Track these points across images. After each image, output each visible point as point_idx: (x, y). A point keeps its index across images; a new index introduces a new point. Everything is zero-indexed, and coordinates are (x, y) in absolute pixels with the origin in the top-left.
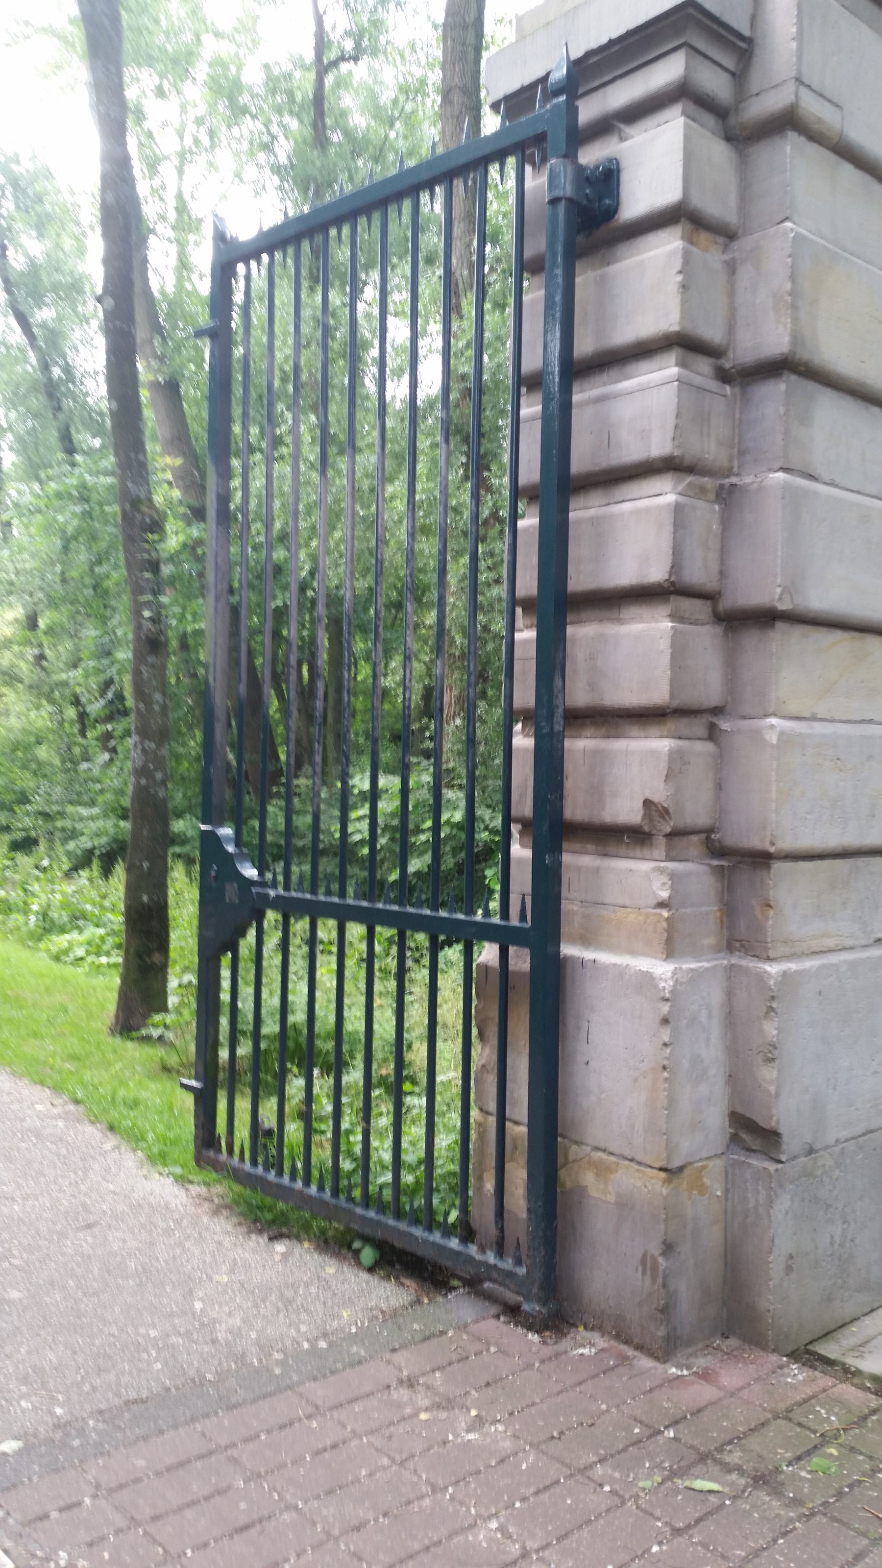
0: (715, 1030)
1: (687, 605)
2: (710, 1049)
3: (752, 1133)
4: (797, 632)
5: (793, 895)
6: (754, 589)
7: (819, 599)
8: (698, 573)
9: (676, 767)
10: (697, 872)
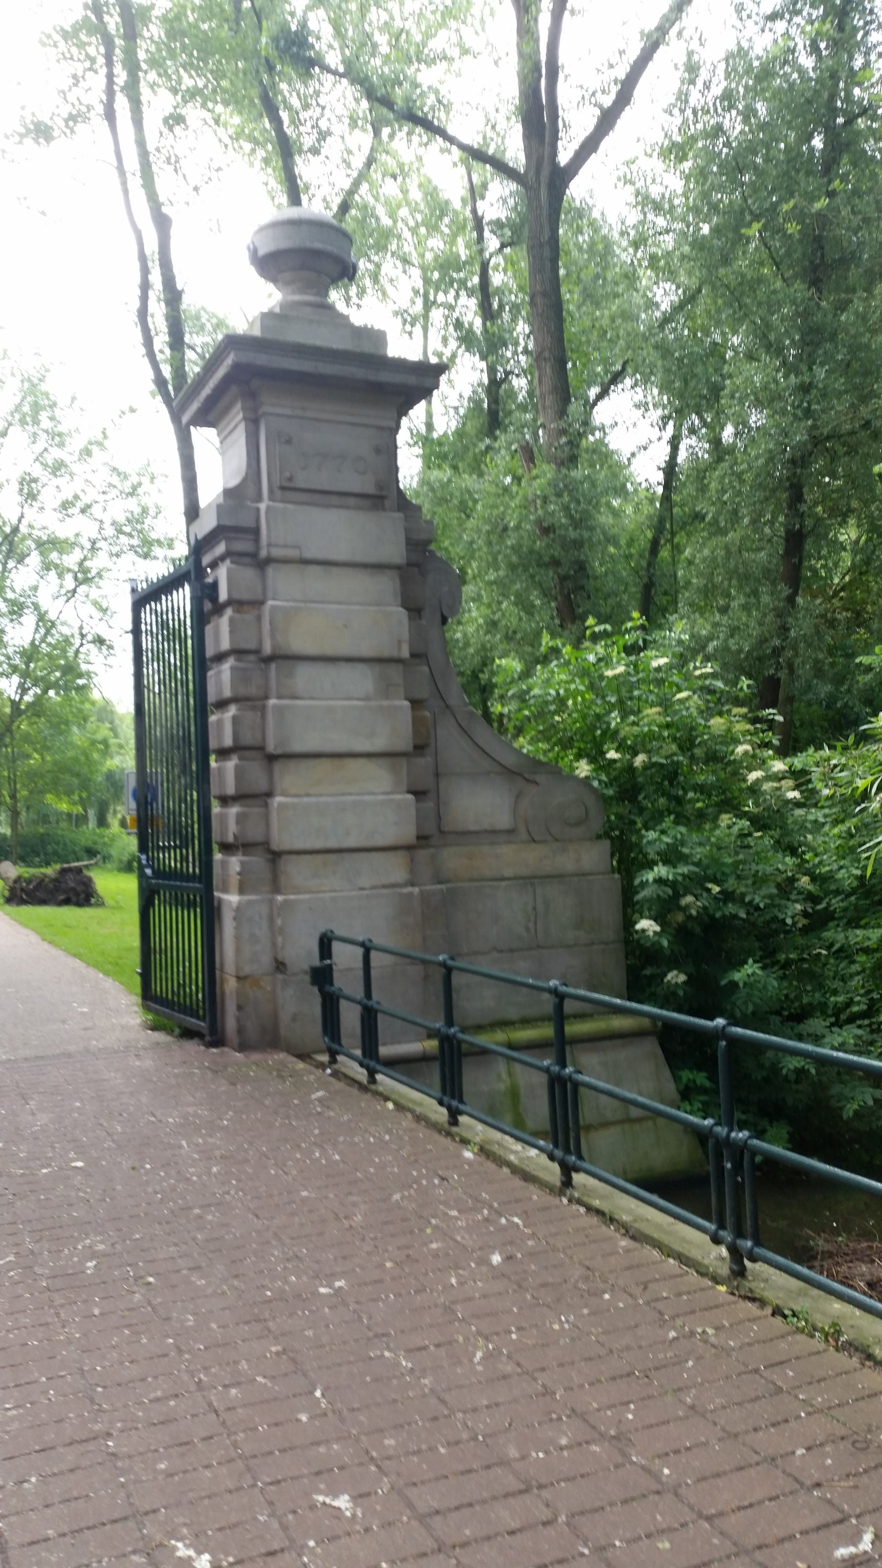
0: (265, 925)
1: (247, 753)
2: (262, 931)
3: (280, 966)
4: (292, 764)
5: (296, 871)
6: (271, 748)
7: (298, 747)
8: (248, 739)
9: (241, 819)
10: (257, 861)
